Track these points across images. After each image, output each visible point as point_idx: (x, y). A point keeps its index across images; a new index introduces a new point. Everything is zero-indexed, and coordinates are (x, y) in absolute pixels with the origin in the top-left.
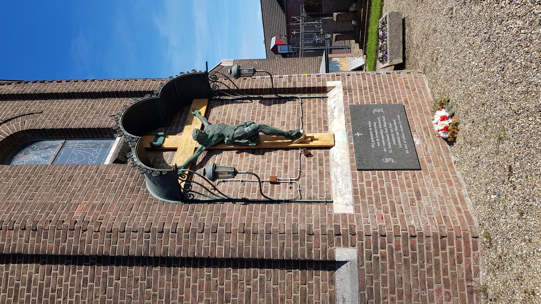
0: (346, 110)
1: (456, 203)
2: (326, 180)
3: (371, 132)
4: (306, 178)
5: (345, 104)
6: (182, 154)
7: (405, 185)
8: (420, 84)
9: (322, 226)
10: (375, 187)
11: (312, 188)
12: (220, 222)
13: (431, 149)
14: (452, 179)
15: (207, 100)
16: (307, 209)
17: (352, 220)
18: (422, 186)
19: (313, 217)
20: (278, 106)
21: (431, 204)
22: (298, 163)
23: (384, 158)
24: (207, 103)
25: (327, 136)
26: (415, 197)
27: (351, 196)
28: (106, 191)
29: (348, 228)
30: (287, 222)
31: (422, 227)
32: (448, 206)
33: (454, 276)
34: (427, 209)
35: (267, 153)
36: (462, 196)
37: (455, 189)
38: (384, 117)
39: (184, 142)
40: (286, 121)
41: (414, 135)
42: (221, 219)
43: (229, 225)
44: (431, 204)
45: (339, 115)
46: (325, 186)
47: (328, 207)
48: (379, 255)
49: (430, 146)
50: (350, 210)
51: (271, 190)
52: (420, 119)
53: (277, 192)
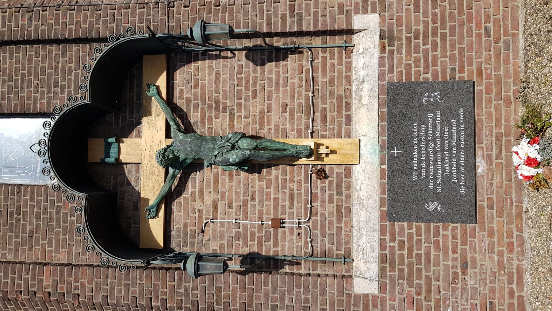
0: (381, 91)
1: (510, 282)
3: (415, 147)
4: (319, 218)
5: (381, 76)
6: (149, 177)
7: (450, 250)
8: (510, 26)
10: (410, 250)
11: (327, 235)
12: (216, 299)
13: (498, 181)
14: (515, 242)
15: (163, 57)
16: (321, 284)
19: (328, 298)
20: (276, 66)
21: (478, 283)
22: (308, 191)
23: (428, 203)
24: (165, 66)
26: (459, 271)
27: (377, 266)
28: (69, 234)
30: (296, 303)
32: (499, 286)
34: (471, 290)
35: (265, 170)
37: (515, 259)
38: (438, 113)
40: (288, 101)
41: (479, 153)
42: (217, 295)
44: (478, 283)
45: (369, 103)
47: (347, 283)
49: (499, 176)
51: (274, 237)
52: (494, 115)
53: (282, 241)
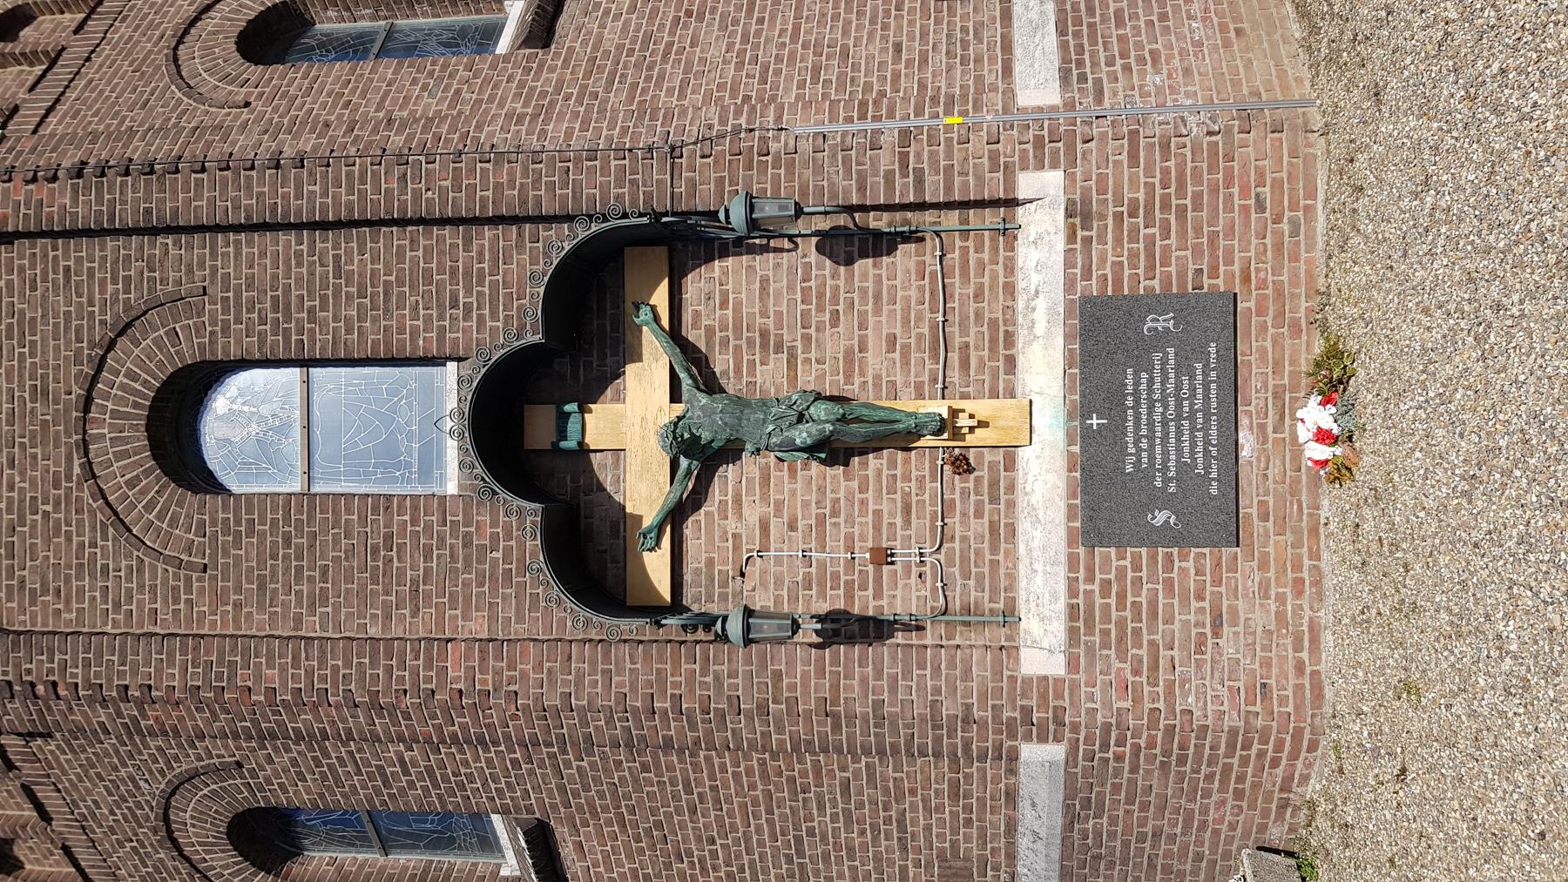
1: (1298, 648)
2: (1007, 553)
3: (1130, 412)
4: (957, 545)
5: (1069, 285)
9: (994, 707)
10: (1121, 597)
11: (973, 576)
14: (1307, 577)
17: (1059, 695)
18: (1232, 598)
19: (974, 684)
20: (875, 265)
24: (666, 269)
25: (1011, 413)
26: (1208, 630)
27: (1062, 627)
29: (1051, 714)
30: (918, 696)
31: (1210, 713)
33: (1256, 786)
36: (1316, 629)
37: (1306, 607)
39: (637, 427)
40: (898, 331)
41: (1244, 421)
43: (792, 702)
46: (1002, 571)
48: (1110, 755)
49: (1278, 462)
50: (1055, 666)
